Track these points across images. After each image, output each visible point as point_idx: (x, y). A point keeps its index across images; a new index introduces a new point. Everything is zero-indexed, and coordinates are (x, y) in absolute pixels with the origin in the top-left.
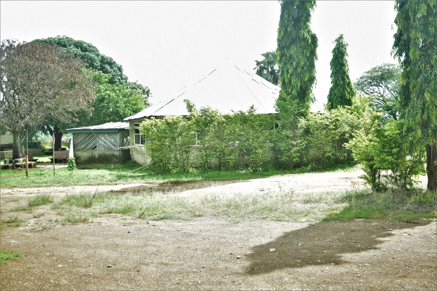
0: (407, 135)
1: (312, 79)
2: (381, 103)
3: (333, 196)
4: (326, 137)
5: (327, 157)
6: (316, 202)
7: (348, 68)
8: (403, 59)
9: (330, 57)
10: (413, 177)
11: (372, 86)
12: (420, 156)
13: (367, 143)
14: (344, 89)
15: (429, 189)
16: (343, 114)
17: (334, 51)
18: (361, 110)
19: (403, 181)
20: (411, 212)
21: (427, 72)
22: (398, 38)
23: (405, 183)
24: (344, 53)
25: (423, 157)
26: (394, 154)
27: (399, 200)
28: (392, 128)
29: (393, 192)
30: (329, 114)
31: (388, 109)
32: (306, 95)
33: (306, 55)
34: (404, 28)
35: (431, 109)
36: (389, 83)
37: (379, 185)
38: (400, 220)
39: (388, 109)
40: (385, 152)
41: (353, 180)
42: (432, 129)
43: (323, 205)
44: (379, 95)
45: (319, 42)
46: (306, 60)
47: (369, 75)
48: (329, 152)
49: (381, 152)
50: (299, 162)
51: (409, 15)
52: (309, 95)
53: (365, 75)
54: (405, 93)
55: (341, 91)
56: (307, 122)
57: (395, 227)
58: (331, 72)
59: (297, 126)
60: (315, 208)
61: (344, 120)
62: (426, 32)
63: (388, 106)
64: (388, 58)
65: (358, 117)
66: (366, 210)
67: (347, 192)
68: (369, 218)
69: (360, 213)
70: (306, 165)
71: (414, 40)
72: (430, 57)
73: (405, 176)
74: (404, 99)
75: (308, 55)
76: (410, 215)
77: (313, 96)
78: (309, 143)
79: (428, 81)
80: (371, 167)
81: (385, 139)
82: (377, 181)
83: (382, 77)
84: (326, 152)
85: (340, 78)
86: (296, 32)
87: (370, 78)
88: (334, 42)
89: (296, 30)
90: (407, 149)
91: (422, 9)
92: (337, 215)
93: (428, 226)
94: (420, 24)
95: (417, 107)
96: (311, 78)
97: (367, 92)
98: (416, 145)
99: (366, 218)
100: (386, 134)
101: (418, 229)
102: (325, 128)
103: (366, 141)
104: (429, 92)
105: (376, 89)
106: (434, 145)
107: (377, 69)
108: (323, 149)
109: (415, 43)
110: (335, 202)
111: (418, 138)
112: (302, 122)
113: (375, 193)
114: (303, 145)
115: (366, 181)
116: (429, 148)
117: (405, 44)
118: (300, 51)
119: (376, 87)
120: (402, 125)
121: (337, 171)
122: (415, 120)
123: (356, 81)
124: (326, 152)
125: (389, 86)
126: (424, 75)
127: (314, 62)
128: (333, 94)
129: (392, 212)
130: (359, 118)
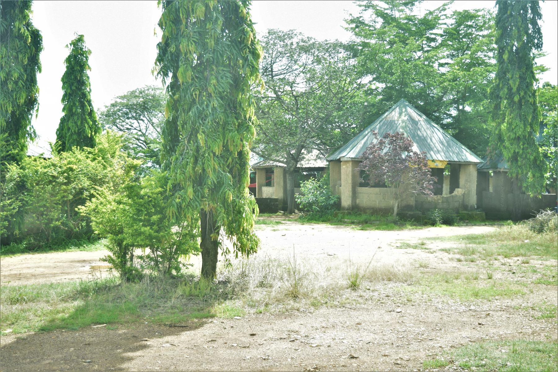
0: (173, 195)
1: (31, 102)
2: (142, 146)
3: (59, 290)
4: (52, 195)
5: (54, 228)
6: (32, 300)
7: (90, 89)
8: (169, 80)
9: (63, 69)
10: (181, 259)
11: (128, 118)
12: (191, 227)
13: (114, 206)
14: (84, 120)
15: (204, 275)
16: (80, 161)
17: (68, 60)
18: (109, 156)
19: (167, 264)
20: (176, 310)
21: (203, 103)
22: (163, 48)
23: (169, 267)
24: (84, 64)
25: (195, 228)
26: (154, 224)
27: (159, 292)
28: (151, 185)
29: (151, 281)
30: (58, 159)
31: (151, 154)
32: (21, 127)
33: (23, 62)
34: (172, 34)
35: (207, 157)
36: (155, 116)
37: (132, 270)
38: (160, 324)
39: (151, 154)
40: (140, 220)
41: (93, 265)
42: (208, 188)
43: (42, 305)
44: (140, 133)
45: (45, 43)
46: (22, 70)
47: (125, 101)
48: (57, 220)
49: (134, 220)
50: (6, 235)
51: (179, 17)
52: (25, 127)
53: (119, 101)
54: (171, 131)
55: (79, 123)
56: (22, 171)
57: (152, 334)
58: (62, 93)
59: (5, 177)
60: (29, 310)
61: (82, 170)
62: (202, 44)
63: (153, 151)
64: (149, 79)
65: (104, 166)
66: (109, 311)
67: (81, 283)
68: (115, 323)
69: (100, 315)
70: (19, 240)
71: (186, 55)
72: (207, 81)
73: (170, 257)
74: (169, 141)
75: (26, 63)
76: (176, 315)
77: (32, 130)
78: (24, 204)
79: (203, 116)
80: (119, 243)
81: (141, 200)
82: (129, 264)
83: (144, 106)
84: (52, 220)
85: (77, 104)
86: (6, 23)
87: (127, 106)
88: (69, 46)
89: (6, 20)
90: (173, 216)
91: (198, 10)
92: (63, 320)
93: (200, 331)
94: (195, 32)
95: (188, 153)
96: (30, 100)
97: (122, 128)
98: (186, 210)
99: (109, 323)
100: (142, 192)
101: (186, 336)
102: (50, 182)
103: (113, 203)
104: (204, 132)
105: (135, 124)
106: (211, 210)
107: (137, 94)
108: (46, 215)
109: (187, 59)
110: (63, 300)
111: (188, 200)
112: (14, 170)
113: (125, 285)
114: (14, 209)
115: (110, 265)
116: (203, 215)
117: (172, 60)
118: (12, 55)
119: (135, 121)
120: (166, 179)
121: (68, 250)
122: (184, 174)
123: (105, 110)
124: (52, 220)
125: (155, 120)
126: (197, 107)
127: (35, 75)
128: (66, 128)
129: (150, 311)
130: (105, 168)
